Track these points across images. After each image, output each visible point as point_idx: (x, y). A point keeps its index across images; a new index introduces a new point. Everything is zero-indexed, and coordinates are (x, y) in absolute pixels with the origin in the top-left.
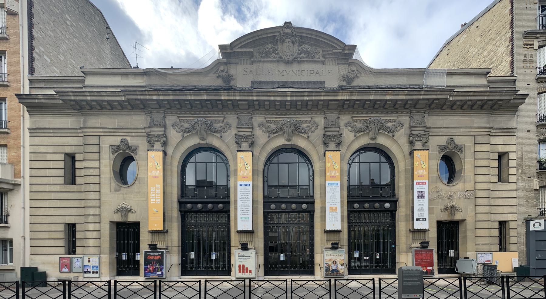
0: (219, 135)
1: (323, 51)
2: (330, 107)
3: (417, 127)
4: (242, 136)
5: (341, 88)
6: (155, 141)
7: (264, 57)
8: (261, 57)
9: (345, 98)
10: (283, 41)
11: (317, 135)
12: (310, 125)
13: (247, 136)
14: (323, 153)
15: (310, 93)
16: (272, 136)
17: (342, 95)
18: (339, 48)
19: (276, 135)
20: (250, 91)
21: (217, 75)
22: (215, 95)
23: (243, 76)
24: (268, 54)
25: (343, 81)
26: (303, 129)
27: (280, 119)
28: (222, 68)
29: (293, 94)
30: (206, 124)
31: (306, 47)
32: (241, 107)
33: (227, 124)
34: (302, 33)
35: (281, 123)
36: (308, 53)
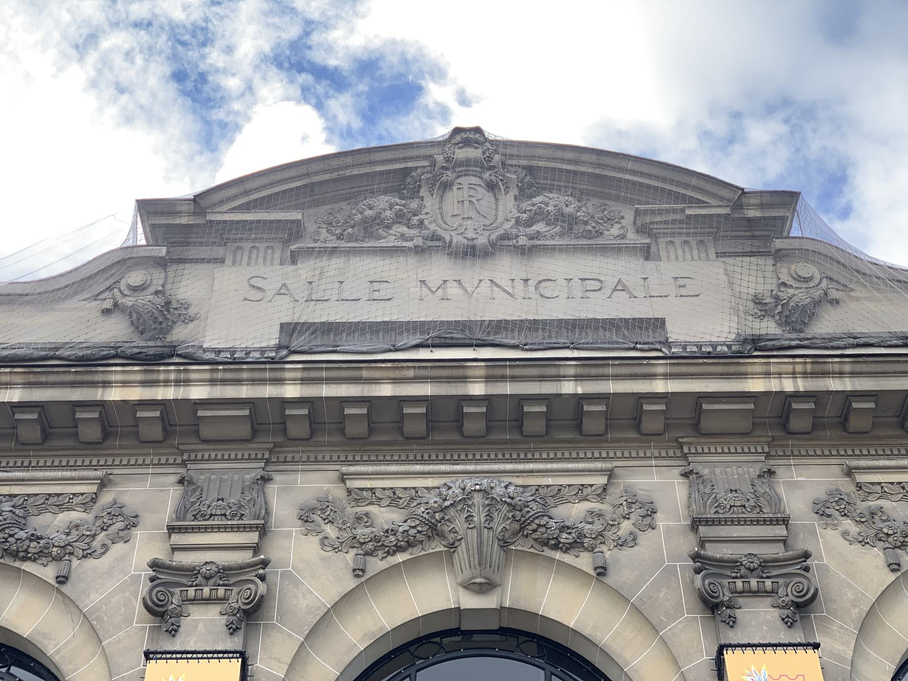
0: (48, 572)
1: (637, 213)
2: (707, 424)
3: (733, 522)
4: (191, 572)
5: (753, 347)
6: (193, 601)
7: (351, 238)
8: (340, 237)
9: (788, 385)
10: (446, 186)
11: (659, 553)
12: (605, 507)
13: (225, 572)
14: (706, 656)
15: (590, 368)
16: (377, 564)
17: (767, 375)
18: (713, 202)
19: (400, 558)
20: (270, 365)
21: (108, 304)
22: (73, 384)
23: (236, 309)
24: (371, 227)
25: (761, 318)
26: (564, 528)
27: (428, 480)
28: (136, 278)
29: (495, 370)
30: (513, 507)
31: (552, 201)
32: (207, 431)
33: (117, 511)
34: (533, 157)
35: (433, 499)
36: (568, 223)
